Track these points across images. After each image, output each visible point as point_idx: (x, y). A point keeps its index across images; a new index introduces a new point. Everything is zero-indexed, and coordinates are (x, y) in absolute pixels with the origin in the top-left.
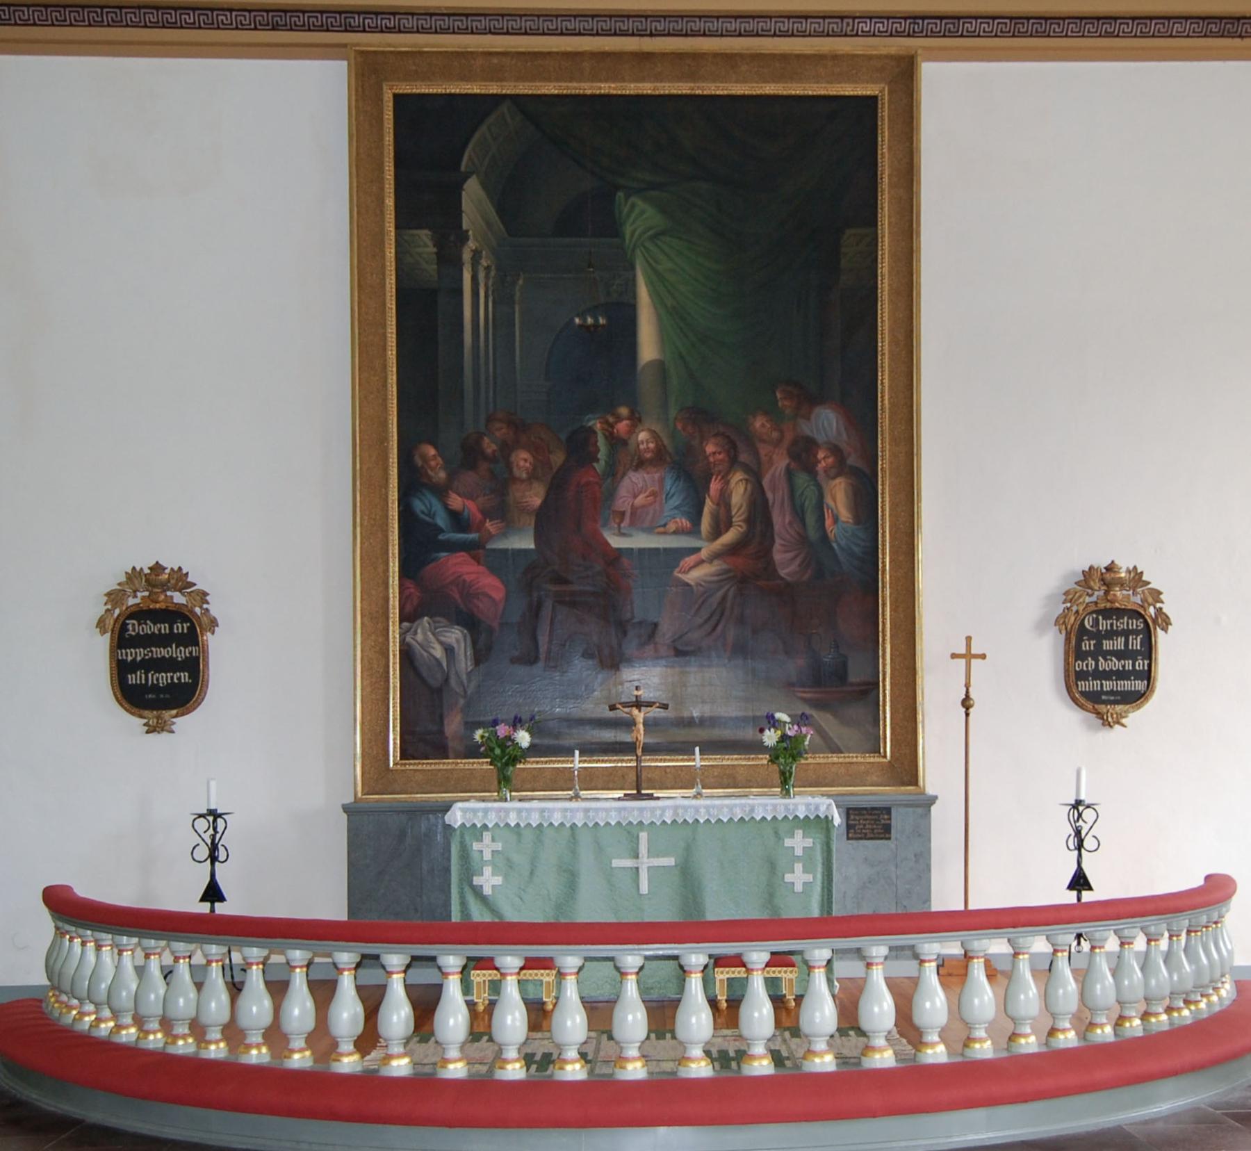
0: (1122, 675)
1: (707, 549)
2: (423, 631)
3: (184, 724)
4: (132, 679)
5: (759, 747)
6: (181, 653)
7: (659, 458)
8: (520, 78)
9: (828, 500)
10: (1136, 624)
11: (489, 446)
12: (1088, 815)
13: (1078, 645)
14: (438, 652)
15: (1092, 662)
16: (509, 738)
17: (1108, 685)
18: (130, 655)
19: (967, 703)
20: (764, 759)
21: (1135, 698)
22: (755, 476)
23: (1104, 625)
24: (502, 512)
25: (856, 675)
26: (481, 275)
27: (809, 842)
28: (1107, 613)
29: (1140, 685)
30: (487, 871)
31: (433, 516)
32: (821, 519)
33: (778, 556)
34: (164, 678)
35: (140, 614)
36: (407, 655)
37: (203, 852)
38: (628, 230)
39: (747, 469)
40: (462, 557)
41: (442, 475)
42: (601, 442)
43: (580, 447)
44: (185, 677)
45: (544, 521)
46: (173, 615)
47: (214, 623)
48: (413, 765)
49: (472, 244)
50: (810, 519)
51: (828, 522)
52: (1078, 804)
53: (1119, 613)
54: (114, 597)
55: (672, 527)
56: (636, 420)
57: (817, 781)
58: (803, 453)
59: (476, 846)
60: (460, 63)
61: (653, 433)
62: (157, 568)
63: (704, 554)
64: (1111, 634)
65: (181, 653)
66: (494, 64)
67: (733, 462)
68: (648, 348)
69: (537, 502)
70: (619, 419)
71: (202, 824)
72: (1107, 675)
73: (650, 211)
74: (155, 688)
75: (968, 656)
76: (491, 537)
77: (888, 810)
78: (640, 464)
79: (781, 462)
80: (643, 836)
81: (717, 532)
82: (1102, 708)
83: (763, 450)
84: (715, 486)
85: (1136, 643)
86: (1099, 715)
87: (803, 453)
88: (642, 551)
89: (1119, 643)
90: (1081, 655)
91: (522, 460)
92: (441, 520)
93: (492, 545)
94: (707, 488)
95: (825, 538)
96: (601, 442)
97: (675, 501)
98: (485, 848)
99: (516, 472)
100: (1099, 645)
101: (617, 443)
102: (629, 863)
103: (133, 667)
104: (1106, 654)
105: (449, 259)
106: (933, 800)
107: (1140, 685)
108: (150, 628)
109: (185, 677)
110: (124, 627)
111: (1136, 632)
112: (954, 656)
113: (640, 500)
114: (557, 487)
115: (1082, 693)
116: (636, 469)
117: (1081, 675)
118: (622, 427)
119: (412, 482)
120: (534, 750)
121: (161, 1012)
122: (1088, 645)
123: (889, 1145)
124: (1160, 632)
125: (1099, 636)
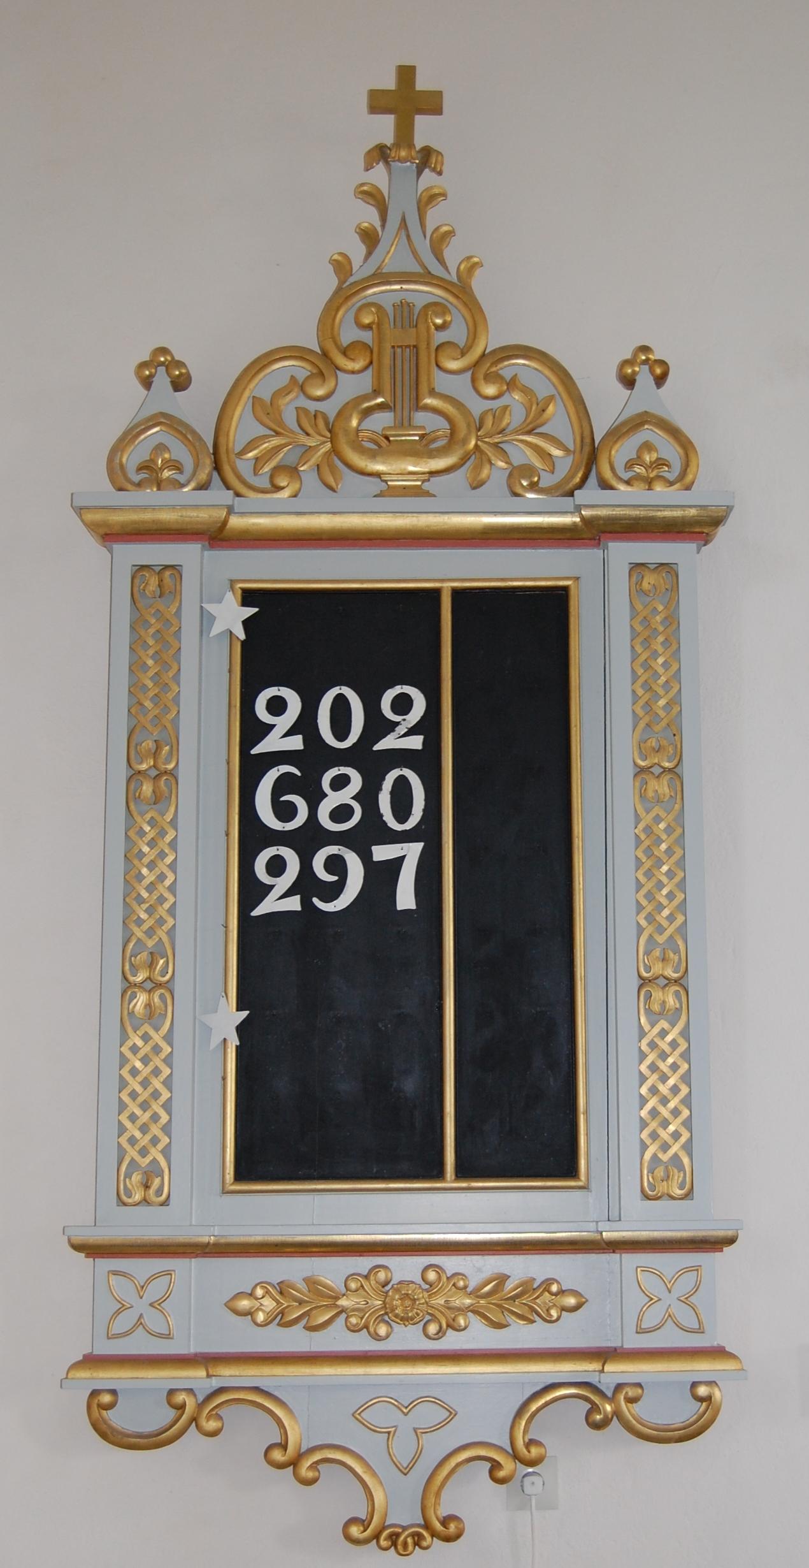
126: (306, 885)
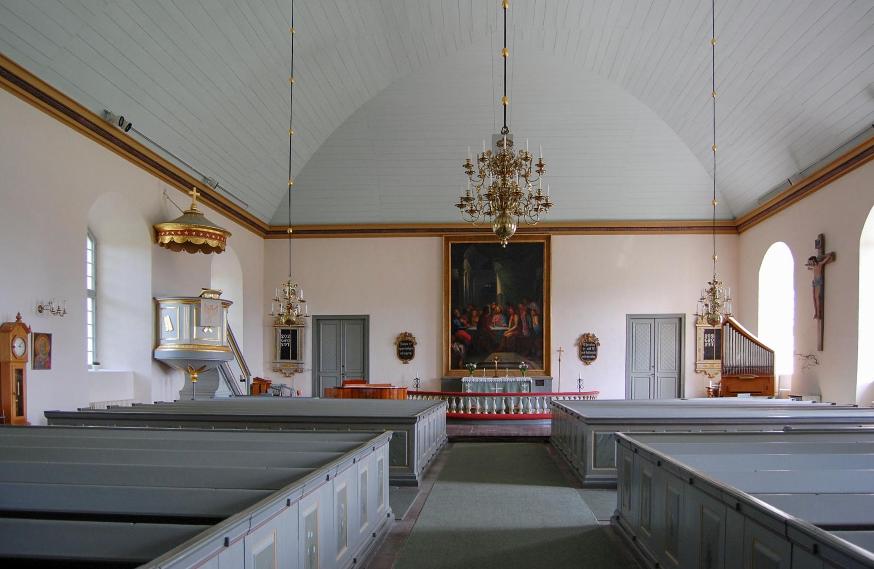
0: (591, 355)
1: (510, 330)
2: (455, 345)
3: (410, 362)
4: (402, 353)
5: (518, 368)
6: (410, 349)
7: (501, 312)
8: (475, 240)
9: (533, 320)
10: (594, 345)
11: (468, 310)
12: (581, 382)
13: (582, 348)
14: (458, 349)
15: (585, 352)
16: (472, 366)
17: (588, 357)
18: (400, 349)
19: (559, 360)
20: (520, 370)
21: (593, 359)
22: (519, 315)
23: (587, 345)
24: (470, 322)
25: (538, 355)
26: (467, 277)
27: (526, 385)
28: (588, 343)
29: (594, 357)
30: (469, 389)
31: (457, 323)
32: (532, 324)
33: (524, 331)
34: (407, 354)
35: (403, 342)
36: (452, 349)
37: (415, 386)
38: (495, 268)
39: (518, 314)
40: (462, 331)
41: (459, 315)
42: (490, 309)
43: (485, 310)
44: (411, 353)
45: (479, 324)
46: (409, 342)
47: (416, 343)
48: (453, 370)
49: (465, 271)
50: (530, 324)
51: (533, 325)
52: (580, 379)
53: (590, 343)
54: (398, 338)
55: (503, 325)
56: (496, 305)
57: (528, 375)
58: (529, 311)
59: (467, 385)
60: (464, 238)
61: (500, 308)
62: (406, 333)
63: (509, 331)
64: (588, 347)
65: (410, 349)
66: (470, 238)
67: (515, 313)
68: (499, 291)
69: (477, 320)
70: (493, 305)
71: (415, 381)
72: (588, 355)
73: (500, 265)
74: (405, 355)
75: (560, 351)
76: (468, 327)
77: (544, 380)
78: (497, 313)
79: (525, 313)
80: (497, 384)
81: (512, 327)
82: (586, 361)
83: (521, 311)
84: (511, 317)
85: (593, 348)
86: (586, 363)
87: (529, 311)
88: (497, 330)
89: (590, 348)
90: (583, 351)
91: (475, 313)
92: (459, 324)
93: (469, 329)
94: (510, 318)
95: (533, 328)
96: (490, 309)
97: (504, 320)
98: (469, 385)
99: (473, 315)
100: (586, 349)
101: (493, 310)
102: (494, 389)
103: (401, 351)
104: (587, 351)
105: (461, 275)
106: (552, 378)
107: (594, 357)
108: (405, 344)
109: (411, 353)
110: (400, 344)
111: (593, 346)
112: (558, 351)
113: (497, 320)
114: (481, 317)
115: (583, 358)
116: (496, 314)
117: (583, 355)
118: (494, 306)
119: (454, 317)
120: (477, 368)
121: (291, 239)
122: (584, 349)
123: (201, 350)
124: (598, 347)
125: (586, 347)
126: (707, 345)
